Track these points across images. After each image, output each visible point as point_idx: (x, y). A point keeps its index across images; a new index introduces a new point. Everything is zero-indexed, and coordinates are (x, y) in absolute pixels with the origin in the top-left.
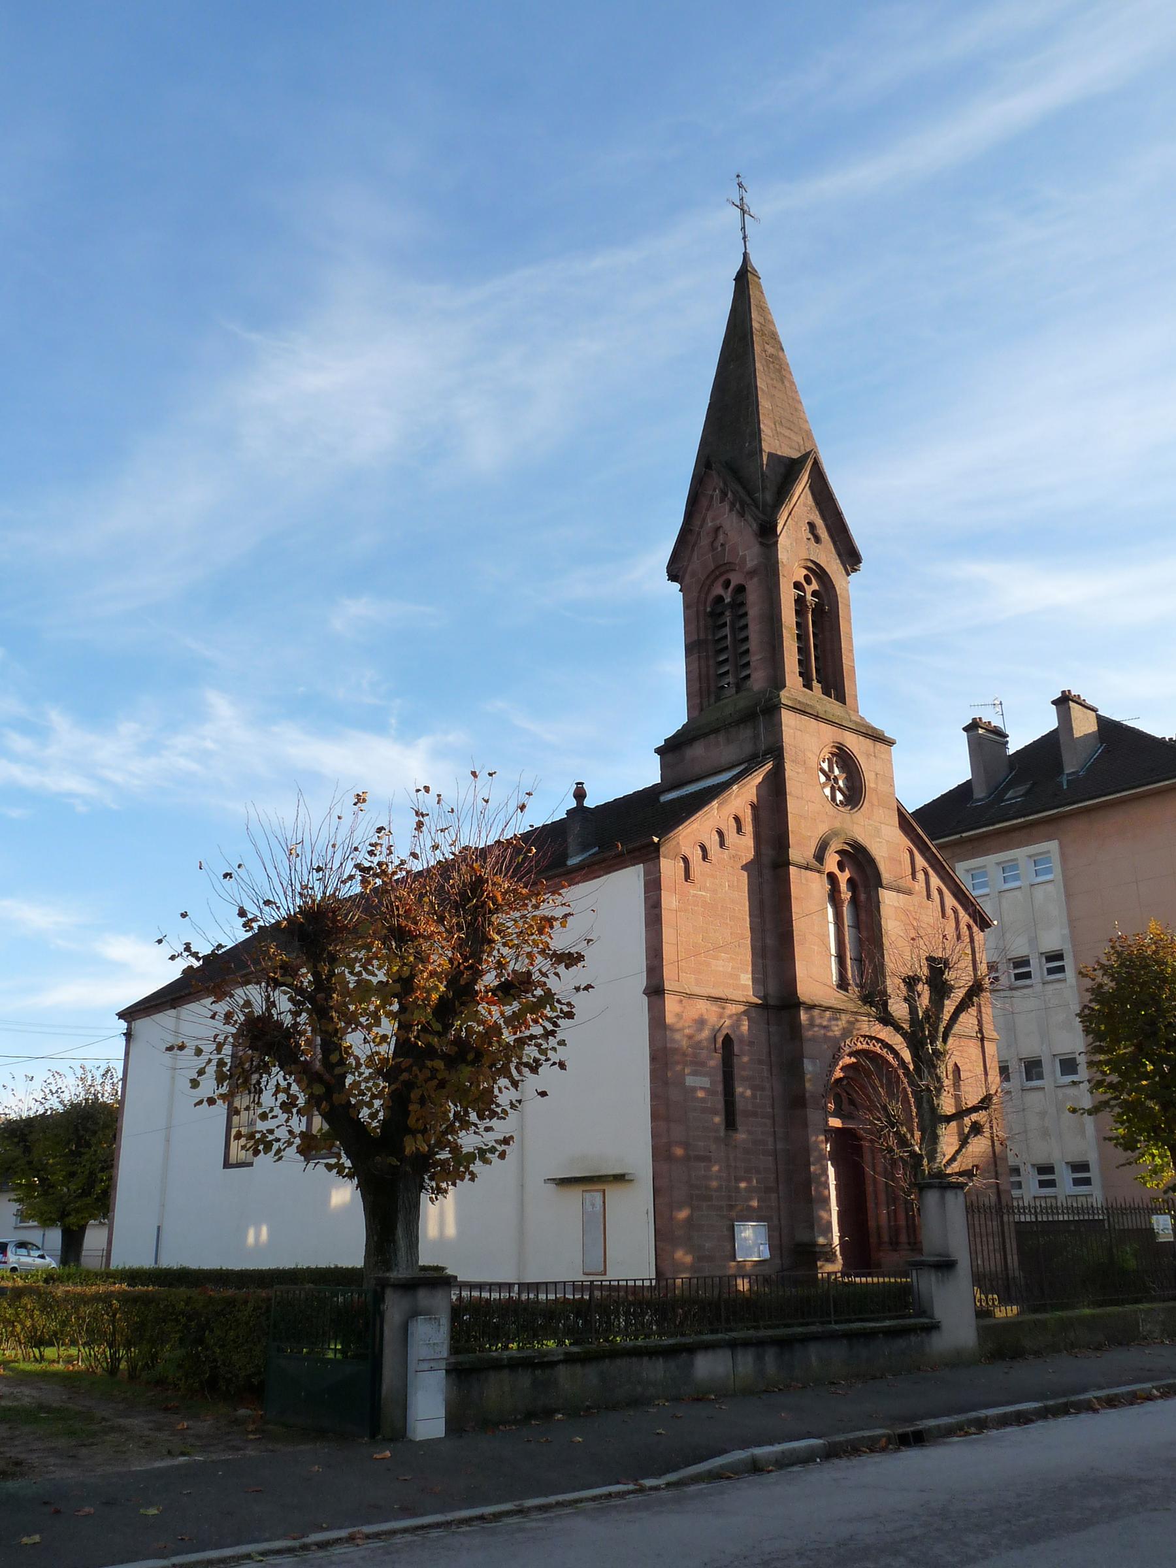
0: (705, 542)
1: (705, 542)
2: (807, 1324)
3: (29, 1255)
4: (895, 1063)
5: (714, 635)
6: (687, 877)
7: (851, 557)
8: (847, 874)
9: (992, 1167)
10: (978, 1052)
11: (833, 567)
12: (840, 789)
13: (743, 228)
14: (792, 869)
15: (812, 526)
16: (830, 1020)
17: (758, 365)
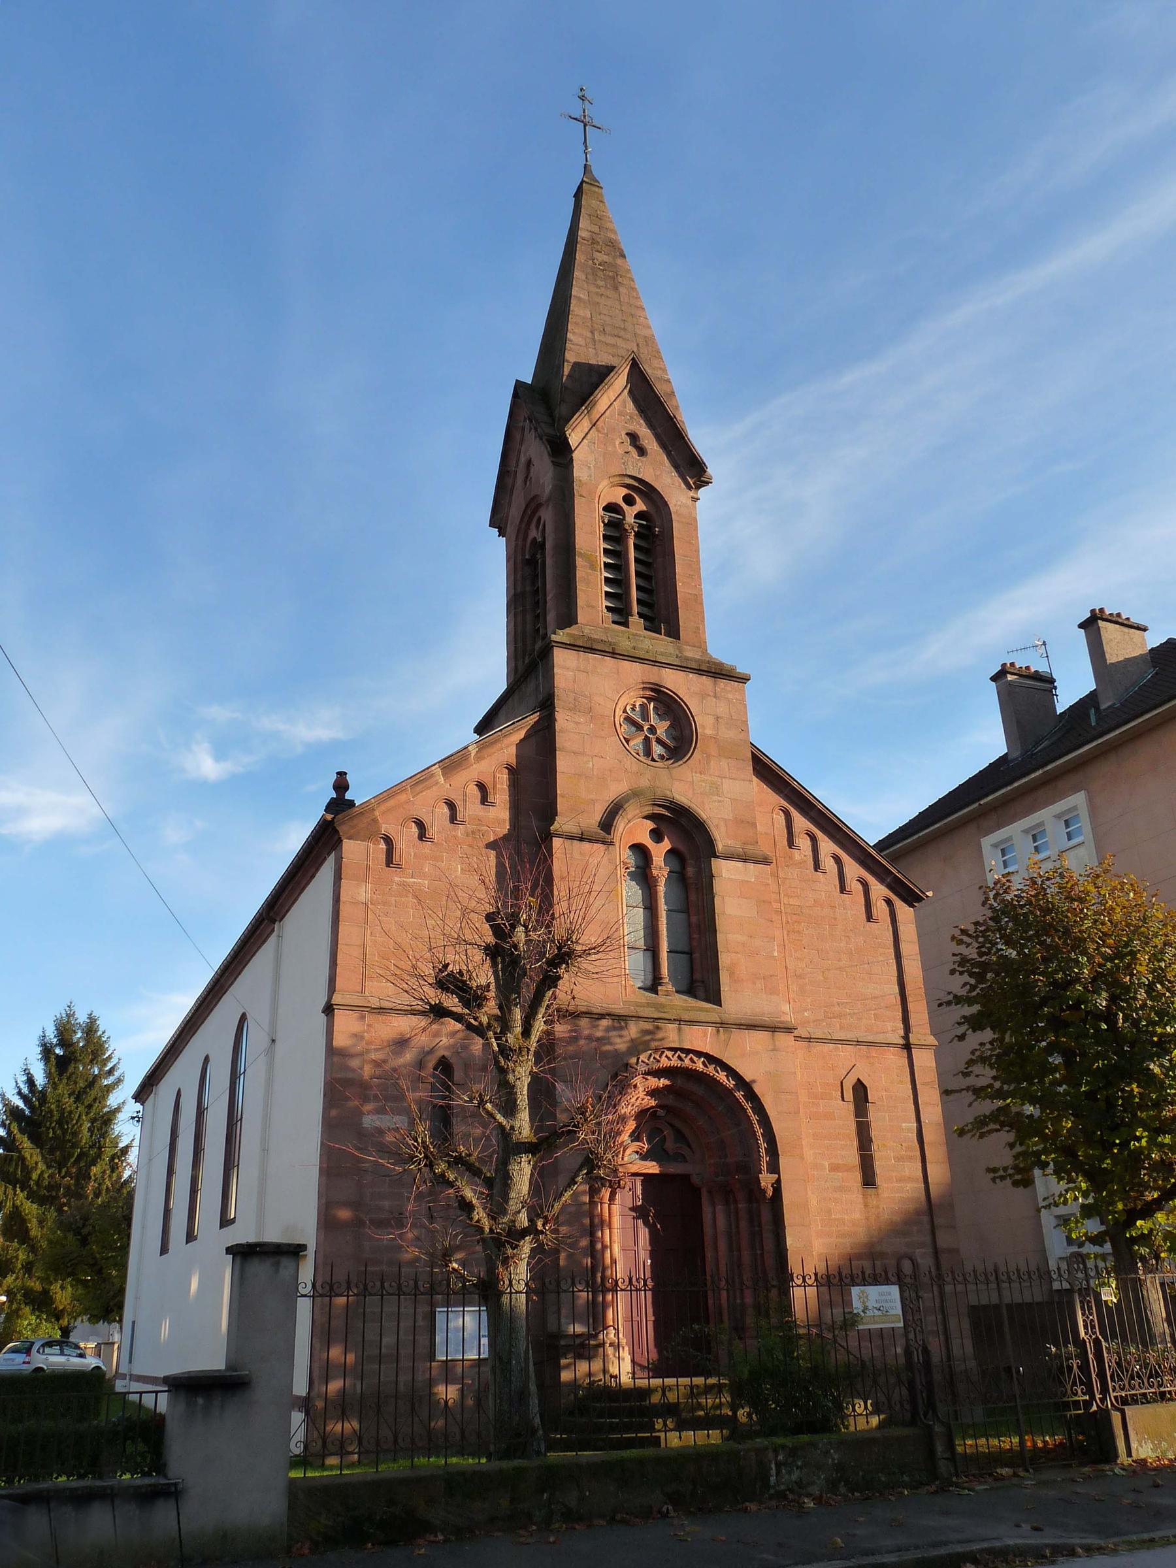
3: (62, 1354)
4: (731, 1084)
6: (389, 861)
7: (693, 470)
8: (666, 845)
9: (926, 1219)
10: (905, 1062)
11: (667, 480)
12: (659, 741)
14: (557, 842)
15: (633, 437)
16: (608, 1029)
17: (577, 274)
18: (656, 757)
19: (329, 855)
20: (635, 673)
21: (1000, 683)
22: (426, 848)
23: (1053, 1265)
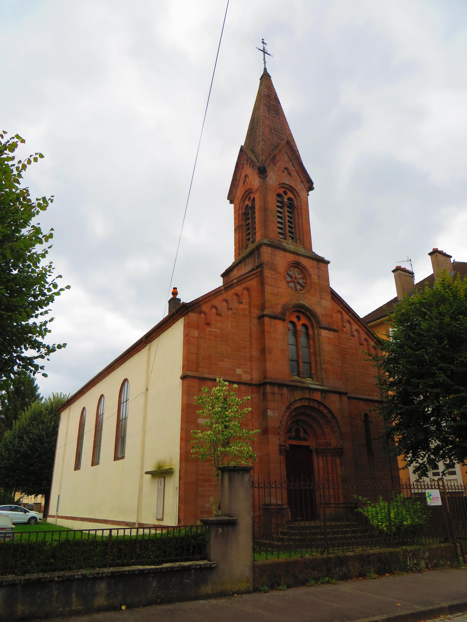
0: (241, 183)
1: (241, 183)
2: (123, 565)
5: (246, 222)
13: (264, 59)
18: (298, 290)
19: (181, 317)
20: (291, 257)
21: (226, 279)
22: (219, 318)
23: (412, 483)
